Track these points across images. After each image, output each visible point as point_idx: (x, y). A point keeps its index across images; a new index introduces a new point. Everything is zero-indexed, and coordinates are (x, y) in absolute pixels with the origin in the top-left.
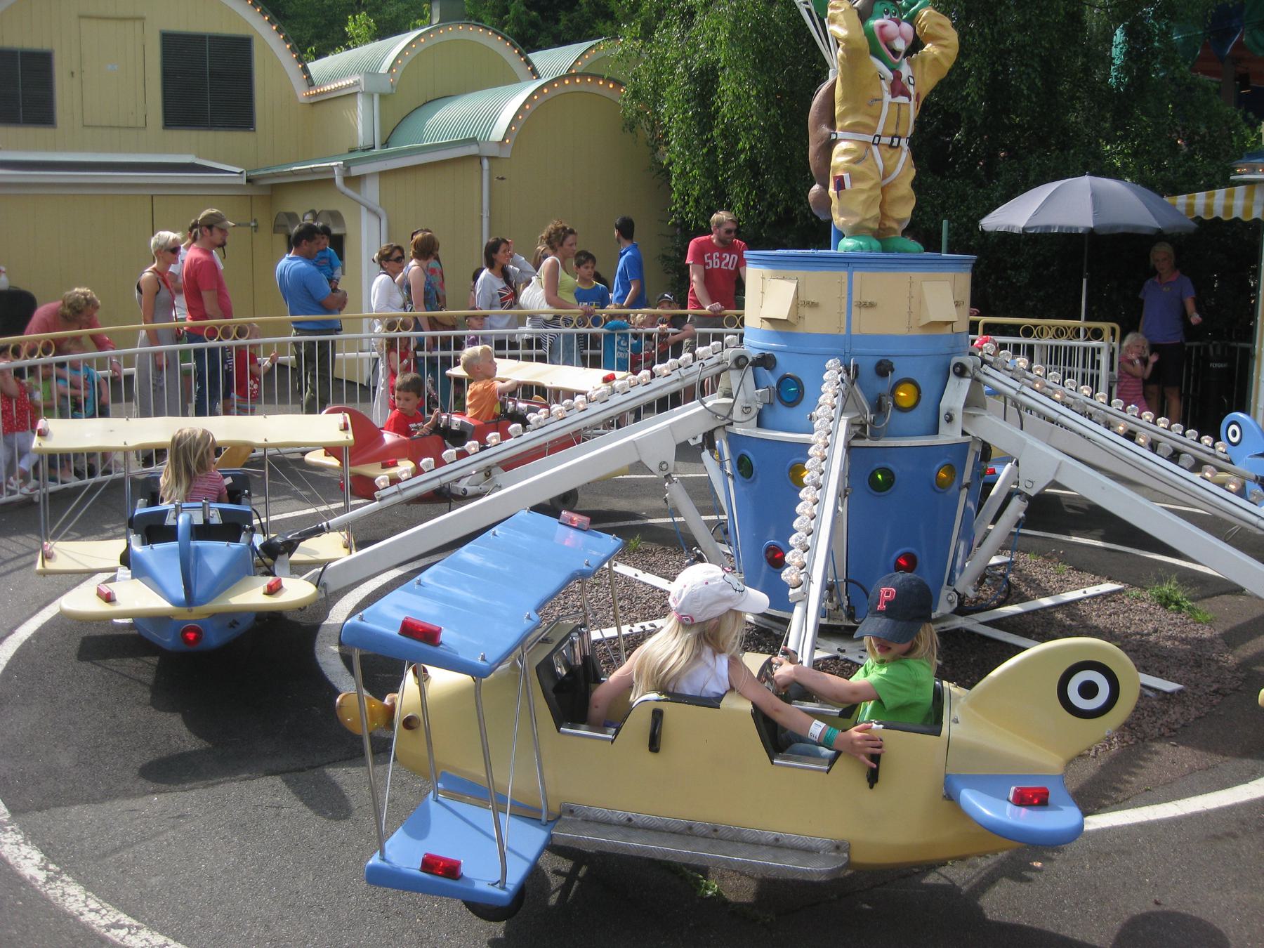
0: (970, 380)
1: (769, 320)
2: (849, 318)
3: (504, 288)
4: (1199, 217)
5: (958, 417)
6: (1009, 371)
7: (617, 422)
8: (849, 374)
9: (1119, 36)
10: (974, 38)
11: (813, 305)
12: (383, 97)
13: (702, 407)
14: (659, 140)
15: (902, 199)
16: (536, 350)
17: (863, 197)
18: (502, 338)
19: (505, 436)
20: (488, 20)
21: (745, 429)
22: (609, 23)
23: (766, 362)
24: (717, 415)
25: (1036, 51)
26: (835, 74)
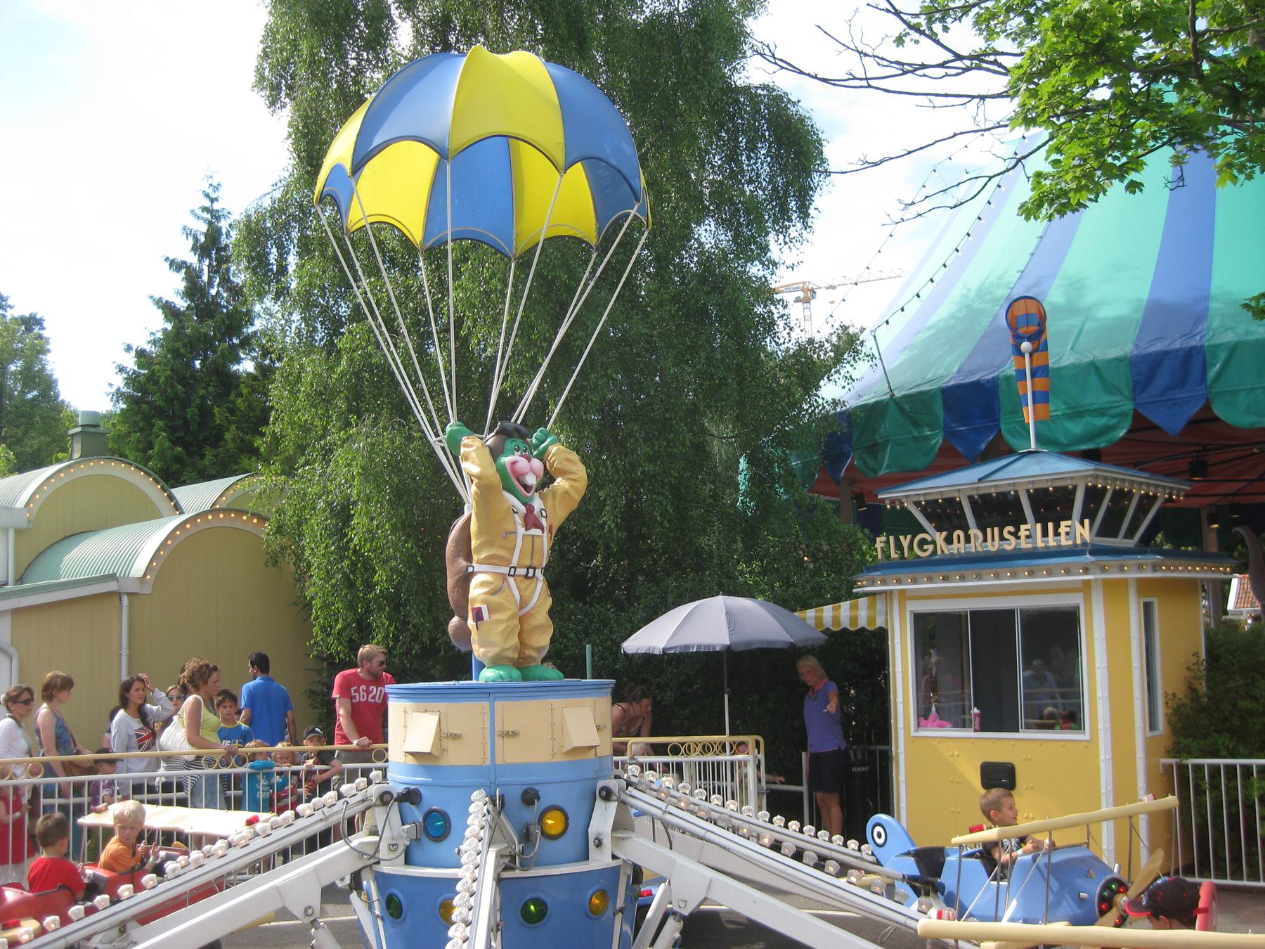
0: (616, 803)
1: (413, 754)
2: (493, 748)
3: (141, 729)
4: (828, 629)
5: (607, 841)
6: (655, 791)
7: (267, 864)
8: (495, 805)
9: (743, 464)
10: (607, 469)
11: (456, 737)
12: (18, 532)
13: (347, 847)
14: (302, 575)
15: (540, 628)
16: (174, 793)
17: (501, 627)
18: (140, 782)
19: (139, 888)
20: (132, 455)
21: (393, 867)
22: (254, 459)
23: (411, 796)
24: (363, 854)
25: (666, 480)
26: (470, 509)
